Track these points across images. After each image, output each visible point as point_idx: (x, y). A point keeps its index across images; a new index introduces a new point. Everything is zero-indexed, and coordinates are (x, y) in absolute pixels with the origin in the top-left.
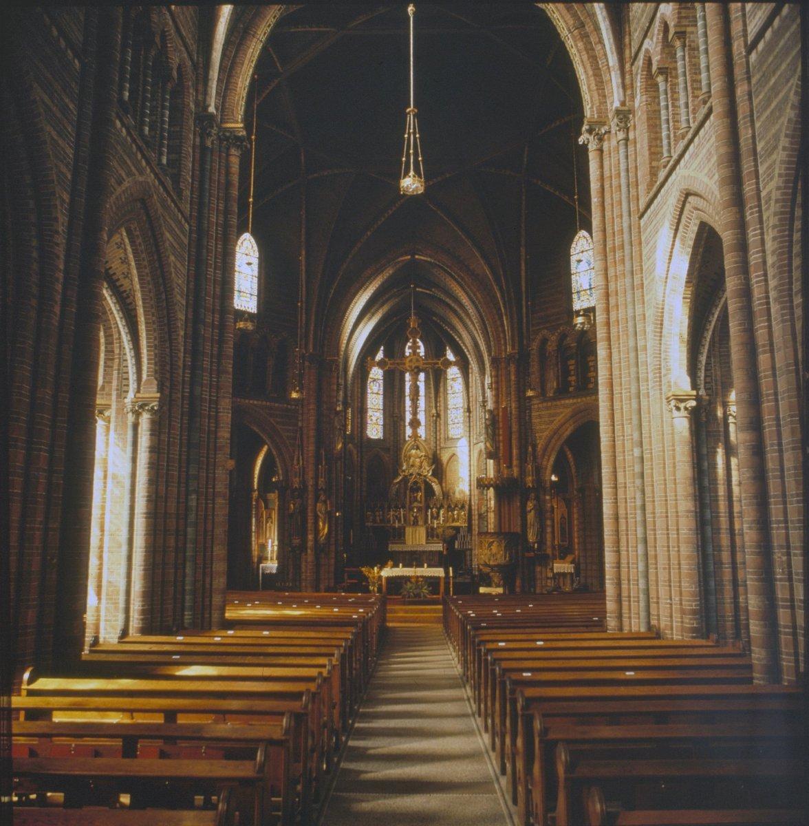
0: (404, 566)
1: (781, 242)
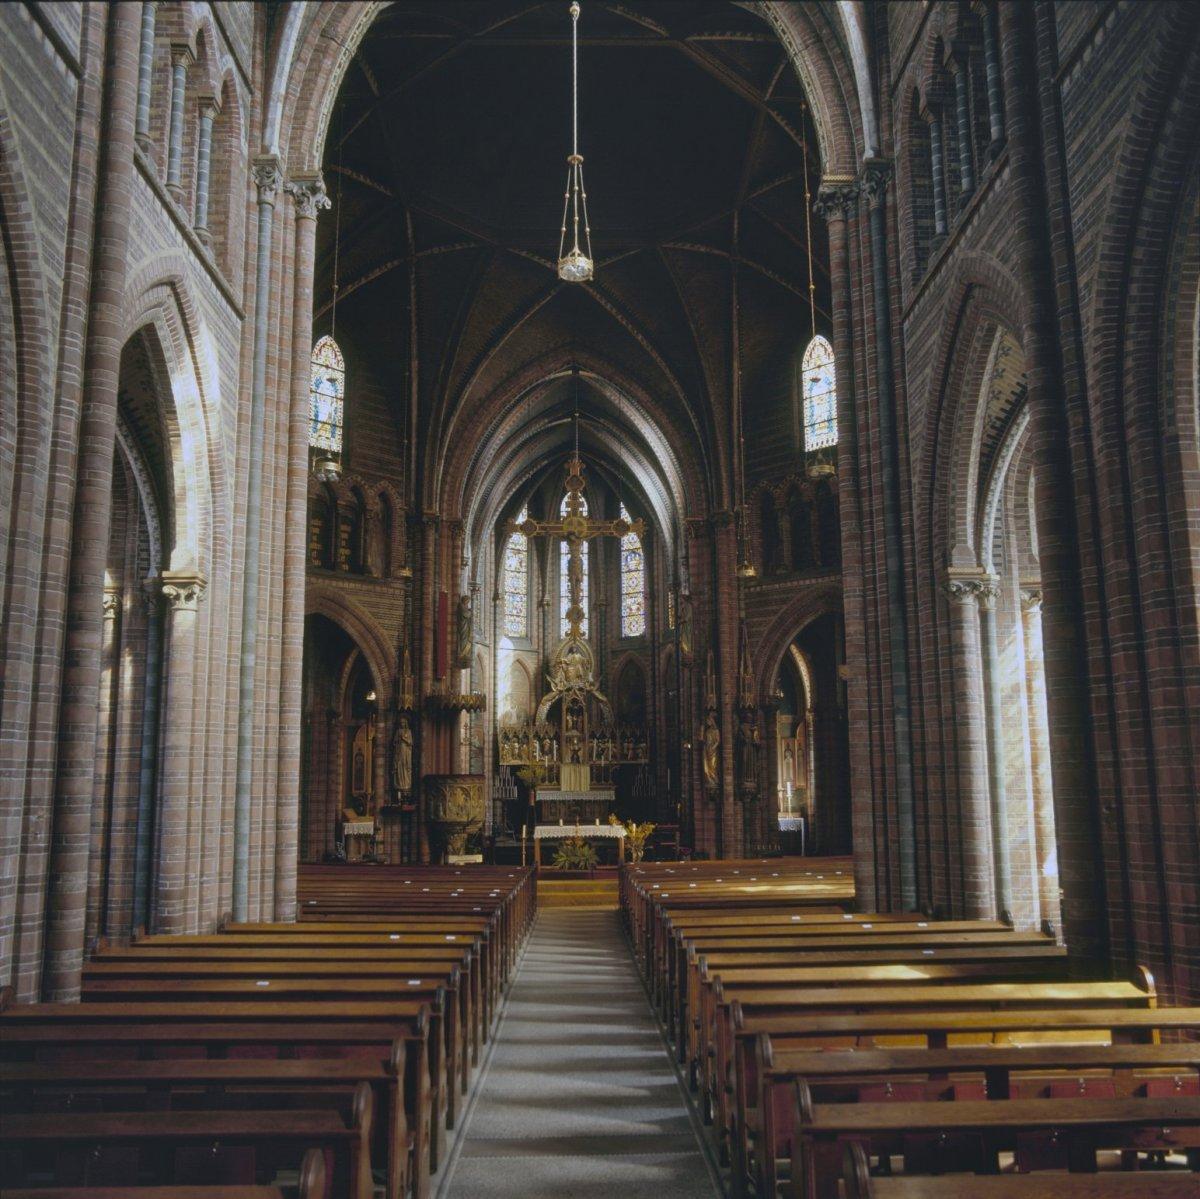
0: (565, 824)
1: (1106, 352)
